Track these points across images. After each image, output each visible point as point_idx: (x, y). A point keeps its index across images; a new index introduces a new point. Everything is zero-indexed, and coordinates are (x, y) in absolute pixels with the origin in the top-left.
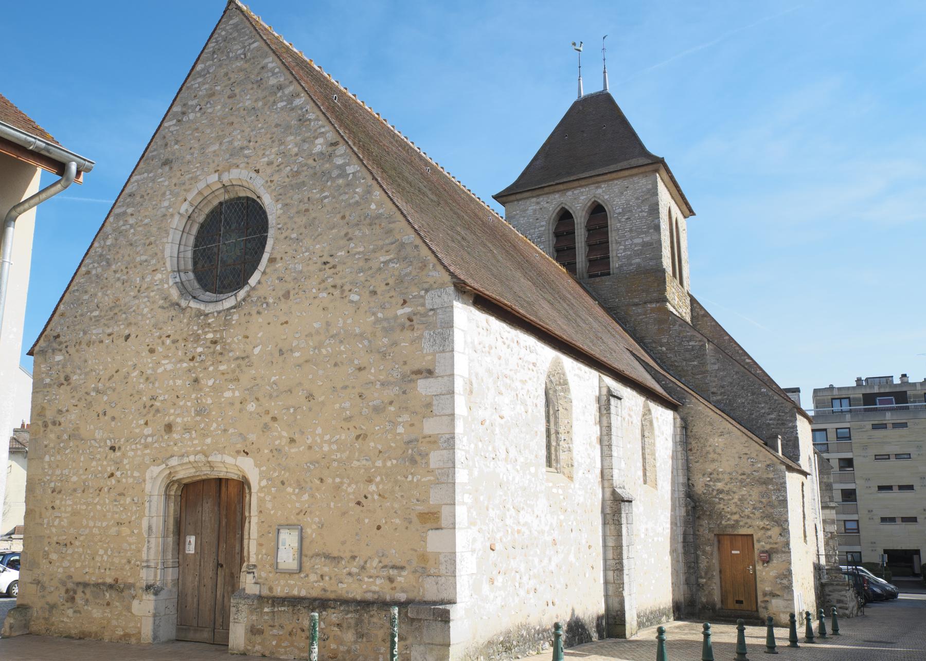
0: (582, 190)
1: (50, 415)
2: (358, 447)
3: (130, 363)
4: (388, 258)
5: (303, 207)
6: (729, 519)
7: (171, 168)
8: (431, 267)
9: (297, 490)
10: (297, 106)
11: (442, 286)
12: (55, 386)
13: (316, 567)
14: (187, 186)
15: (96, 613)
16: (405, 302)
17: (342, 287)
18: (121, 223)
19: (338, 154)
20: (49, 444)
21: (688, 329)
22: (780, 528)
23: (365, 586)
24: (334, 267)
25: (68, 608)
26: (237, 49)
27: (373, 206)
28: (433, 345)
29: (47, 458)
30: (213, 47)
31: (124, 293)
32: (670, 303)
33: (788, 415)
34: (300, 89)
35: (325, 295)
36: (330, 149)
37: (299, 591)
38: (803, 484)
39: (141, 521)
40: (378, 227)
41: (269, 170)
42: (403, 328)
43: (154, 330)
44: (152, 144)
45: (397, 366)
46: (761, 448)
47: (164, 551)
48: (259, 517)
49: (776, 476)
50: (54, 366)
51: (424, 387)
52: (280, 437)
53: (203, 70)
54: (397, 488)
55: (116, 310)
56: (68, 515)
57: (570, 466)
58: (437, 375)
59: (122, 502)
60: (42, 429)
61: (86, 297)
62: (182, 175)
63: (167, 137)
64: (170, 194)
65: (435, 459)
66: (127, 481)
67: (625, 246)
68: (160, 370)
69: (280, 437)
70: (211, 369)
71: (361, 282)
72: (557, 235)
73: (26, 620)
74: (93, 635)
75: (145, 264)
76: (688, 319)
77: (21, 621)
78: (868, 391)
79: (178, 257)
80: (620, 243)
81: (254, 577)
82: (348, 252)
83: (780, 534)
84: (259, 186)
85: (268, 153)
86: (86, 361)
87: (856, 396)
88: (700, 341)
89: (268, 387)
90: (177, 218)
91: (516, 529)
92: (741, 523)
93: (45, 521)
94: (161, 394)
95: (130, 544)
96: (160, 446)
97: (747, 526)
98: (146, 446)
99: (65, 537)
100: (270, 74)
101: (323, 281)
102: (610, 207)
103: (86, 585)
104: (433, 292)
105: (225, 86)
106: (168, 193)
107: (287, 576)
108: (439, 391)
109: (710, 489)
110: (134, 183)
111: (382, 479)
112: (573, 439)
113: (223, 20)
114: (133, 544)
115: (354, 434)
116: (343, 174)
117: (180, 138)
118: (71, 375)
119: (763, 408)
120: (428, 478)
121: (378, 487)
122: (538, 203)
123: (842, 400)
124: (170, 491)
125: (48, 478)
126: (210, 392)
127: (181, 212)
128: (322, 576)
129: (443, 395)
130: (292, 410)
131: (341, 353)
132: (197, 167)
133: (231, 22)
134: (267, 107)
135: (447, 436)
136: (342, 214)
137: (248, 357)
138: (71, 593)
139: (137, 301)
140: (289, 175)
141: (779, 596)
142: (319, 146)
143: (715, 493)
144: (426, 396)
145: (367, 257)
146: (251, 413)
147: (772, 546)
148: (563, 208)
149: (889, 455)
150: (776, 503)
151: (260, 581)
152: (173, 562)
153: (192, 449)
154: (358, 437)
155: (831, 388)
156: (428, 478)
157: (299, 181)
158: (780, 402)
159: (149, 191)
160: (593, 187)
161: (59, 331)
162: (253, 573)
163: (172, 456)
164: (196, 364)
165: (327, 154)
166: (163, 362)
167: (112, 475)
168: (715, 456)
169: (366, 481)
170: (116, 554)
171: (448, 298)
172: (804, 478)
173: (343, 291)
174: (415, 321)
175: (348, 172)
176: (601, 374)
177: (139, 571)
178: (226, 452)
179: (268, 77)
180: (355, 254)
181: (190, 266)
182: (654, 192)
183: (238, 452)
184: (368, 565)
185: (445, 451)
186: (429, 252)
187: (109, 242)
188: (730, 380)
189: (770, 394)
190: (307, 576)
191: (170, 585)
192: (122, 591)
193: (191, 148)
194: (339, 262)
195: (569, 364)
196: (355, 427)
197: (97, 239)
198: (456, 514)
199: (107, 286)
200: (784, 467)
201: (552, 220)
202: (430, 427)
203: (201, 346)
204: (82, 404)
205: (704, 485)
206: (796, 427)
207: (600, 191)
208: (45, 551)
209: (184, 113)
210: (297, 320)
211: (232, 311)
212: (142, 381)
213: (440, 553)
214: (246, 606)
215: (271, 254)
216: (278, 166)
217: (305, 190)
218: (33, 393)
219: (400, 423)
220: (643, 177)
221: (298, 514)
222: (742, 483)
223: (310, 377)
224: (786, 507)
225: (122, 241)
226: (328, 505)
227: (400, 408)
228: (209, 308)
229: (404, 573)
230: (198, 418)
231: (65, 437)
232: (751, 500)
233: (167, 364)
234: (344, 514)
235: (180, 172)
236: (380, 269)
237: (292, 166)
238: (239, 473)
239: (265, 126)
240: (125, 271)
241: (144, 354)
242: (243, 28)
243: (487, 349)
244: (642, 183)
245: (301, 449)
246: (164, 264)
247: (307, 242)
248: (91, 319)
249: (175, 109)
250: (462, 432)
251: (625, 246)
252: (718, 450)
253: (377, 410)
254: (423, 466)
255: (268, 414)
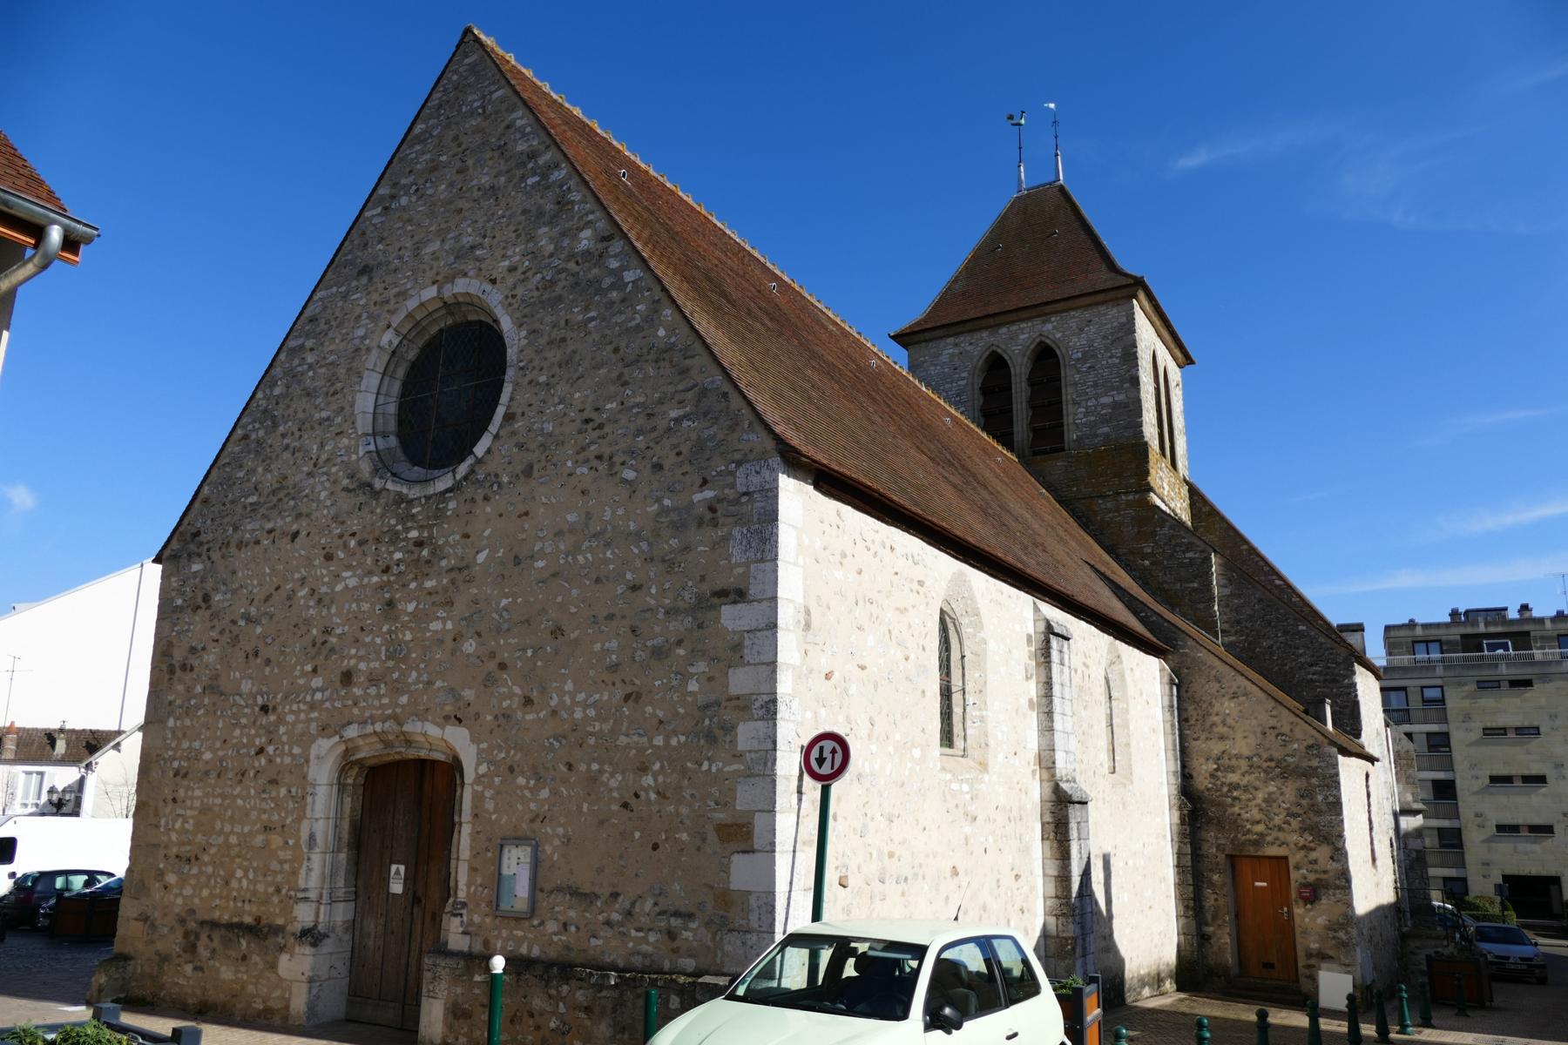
0: (1021, 326)
1: (178, 655)
2: (627, 713)
3: (297, 576)
4: (681, 412)
5: (557, 334)
6: (1249, 831)
7: (370, 279)
8: (746, 426)
9: (532, 782)
10: (554, 182)
11: (763, 457)
12: (189, 611)
13: (557, 909)
14: (392, 306)
15: (227, 973)
16: (705, 482)
17: (611, 458)
18: (296, 362)
19: (612, 253)
20: (175, 701)
21: (1182, 533)
22: (1331, 847)
23: (631, 944)
24: (601, 426)
25: (186, 963)
26: (474, 100)
27: (661, 333)
28: (746, 551)
29: (171, 723)
30: (440, 98)
31: (294, 467)
32: (1155, 494)
33: (1342, 666)
34: (560, 157)
35: (585, 470)
36: (600, 246)
37: (530, 949)
38: (1367, 776)
39: (300, 824)
40: (667, 364)
41: (510, 280)
42: (700, 523)
43: (334, 525)
44: (347, 243)
45: (690, 584)
46: (1298, 719)
47: (333, 874)
48: (473, 824)
49: (1322, 764)
50: (189, 578)
51: (732, 617)
52: (511, 696)
53: (424, 132)
54: (686, 782)
55: (281, 495)
56: (195, 813)
57: (983, 745)
58: (751, 598)
59: (274, 794)
60: (167, 676)
61: (241, 474)
62: (386, 289)
63: (368, 232)
64: (368, 318)
65: (746, 734)
66: (282, 762)
67: (1087, 408)
68: (339, 588)
69: (511, 696)
70: (413, 585)
71: (640, 449)
72: (985, 391)
73: (124, 979)
74: (220, 1008)
75: (326, 423)
76: (1185, 517)
77: (116, 979)
78: (1469, 630)
79: (374, 413)
80: (1079, 404)
81: (462, 922)
82: (622, 403)
83: (1332, 858)
84: (495, 303)
85: (509, 253)
86: (234, 572)
87: (1452, 638)
88: (1202, 551)
89: (495, 616)
90: (375, 352)
91: (886, 852)
92: (1269, 839)
93: (163, 822)
94: (338, 625)
95: (281, 862)
96: (333, 706)
97: (1278, 842)
98: (313, 706)
99: (188, 848)
100: (518, 136)
101: (583, 449)
102: (1064, 351)
103: (214, 925)
104: (748, 466)
105: (454, 155)
106: (364, 316)
107: (513, 923)
108: (754, 625)
109: (1219, 783)
110: (317, 301)
111: (662, 767)
112: (988, 703)
113: (456, 58)
114: (286, 861)
115: (620, 693)
116: (619, 285)
117: (385, 234)
118: (212, 594)
119: (1301, 655)
120: (735, 767)
121: (656, 780)
122: (956, 345)
123: (1430, 644)
124: (346, 779)
125: (170, 753)
126: (410, 621)
127: (382, 344)
128: (565, 925)
129: (760, 630)
130: (529, 653)
131: (606, 561)
132: (408, 277)
133: (467, 61)
134: (512, 184)
135: (766, 698)
136: (614, 345)
137: (467, 567)
138: (192, 938)
139: (311, 481)
140: (540, 286)
141: (1332, 958)
142: (585, 242)
143: (1225, 789)
144: (734, 632)
145: (650, 411)
146: (468, 656)
147: (1318, 876)
148: (994, 352)
149: (1505, 729)
150: (1324, 808)
151: (470, 929)
152: (345, 893)
153: (380, 712)
154: (627, 698)
155: (1412, 625)
156: (735, 767)
157: (554, 294)
158: (1329, 646)
159: (337, 314)
160: (1038, 321)
161: (199, 525)
162: (461, 915)
163: (349, 723)
164: (392, 578)
165: (597, 253)
166: (345, 574)
167: (261, 751)
168: (1224, 730)
169: (638, 769)
170: (261, 878)
171: (770, 476)
172: (1370, 764)
173: (612, 465)
174: (719, 513)
175: (626, 281)
176: (1037, 600)
177: (292, 907)
178: (430, 718)
179: (515, 141)
180: (633, 407)
181: (392, 425)
182: (1129, 327)
183: (447, 718)
184: (637, 909)
185: (760, 723)
186: (743, 404)
187: (277, 391)
188: (1249, 612)
189: (1313, 634)
190: (542, 923)
191: (340, 930)
192: (265, 938)
193: (400, 249)
194: (609, 420)
195: (980, 582)
196: (623, 681)
197: (262, 385)
198: (777, 827)
199: (270, 458)
200: (1335, 750)
201: (977, 371)
202: (740, 681)
203: (399, 550)
204: (225, 639)
205: (1208, 775)
206: (1354, 685)
207: (1049, 326)
208: (159, 869)
209: (393, 197)
210: (542, 510)
211: (448, 495)
212: (312, 603)
213: (750, 893)
214: (447, 970)
215: (508, 407)
216: (524, 273)
217: (561, 310)
218: (158, 620)
219: (693, 675)
220: (1113, 306)
221: (532, 821)
222: (1268, 774)
223: (559, 599)
224: (1340, 813)
225: (296, 390)
226: (579, 808)
227: (693, 651)
228: (414, 492)
229: (693, 925)
230: (391, 663)
231: (199, 689)
232: (1283, 802)
233: (349, 578)
234: (602, 822)
235: (383, 285)
236: (670, 429)
237: (545, 273)
238: (449, 752)
239: (507, 213)
240: (297, 434)
241: (317, 562)
242: (483, 70)
243: (838, 558)
244: (1112, 314)
245: (541, 715)
246: (353, 423)
247: (562, 389)
248: (245, 507)
249: (381, 191)
250: (790, 691)
251: (1087, 408)
252: (1230, 721)
253: (659, 653)
254: (727, 747)
255: (494, 657)
